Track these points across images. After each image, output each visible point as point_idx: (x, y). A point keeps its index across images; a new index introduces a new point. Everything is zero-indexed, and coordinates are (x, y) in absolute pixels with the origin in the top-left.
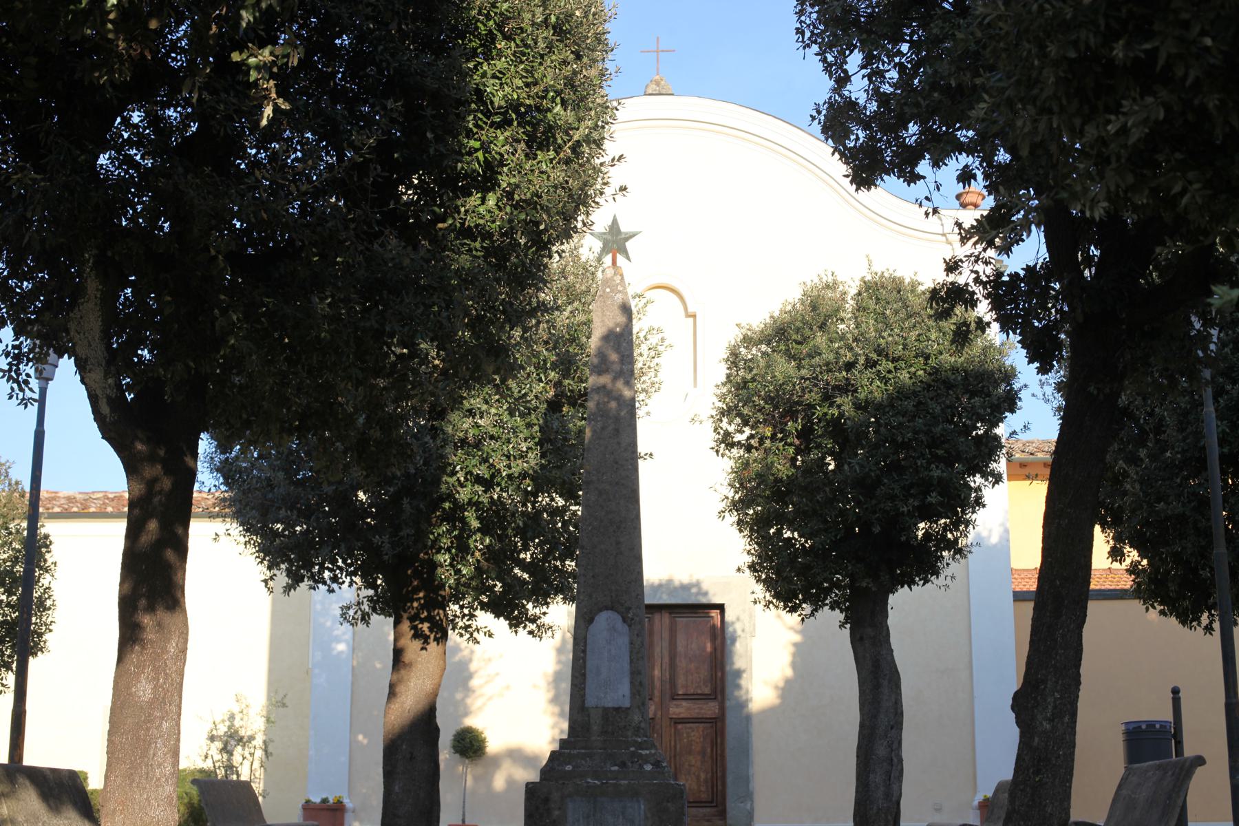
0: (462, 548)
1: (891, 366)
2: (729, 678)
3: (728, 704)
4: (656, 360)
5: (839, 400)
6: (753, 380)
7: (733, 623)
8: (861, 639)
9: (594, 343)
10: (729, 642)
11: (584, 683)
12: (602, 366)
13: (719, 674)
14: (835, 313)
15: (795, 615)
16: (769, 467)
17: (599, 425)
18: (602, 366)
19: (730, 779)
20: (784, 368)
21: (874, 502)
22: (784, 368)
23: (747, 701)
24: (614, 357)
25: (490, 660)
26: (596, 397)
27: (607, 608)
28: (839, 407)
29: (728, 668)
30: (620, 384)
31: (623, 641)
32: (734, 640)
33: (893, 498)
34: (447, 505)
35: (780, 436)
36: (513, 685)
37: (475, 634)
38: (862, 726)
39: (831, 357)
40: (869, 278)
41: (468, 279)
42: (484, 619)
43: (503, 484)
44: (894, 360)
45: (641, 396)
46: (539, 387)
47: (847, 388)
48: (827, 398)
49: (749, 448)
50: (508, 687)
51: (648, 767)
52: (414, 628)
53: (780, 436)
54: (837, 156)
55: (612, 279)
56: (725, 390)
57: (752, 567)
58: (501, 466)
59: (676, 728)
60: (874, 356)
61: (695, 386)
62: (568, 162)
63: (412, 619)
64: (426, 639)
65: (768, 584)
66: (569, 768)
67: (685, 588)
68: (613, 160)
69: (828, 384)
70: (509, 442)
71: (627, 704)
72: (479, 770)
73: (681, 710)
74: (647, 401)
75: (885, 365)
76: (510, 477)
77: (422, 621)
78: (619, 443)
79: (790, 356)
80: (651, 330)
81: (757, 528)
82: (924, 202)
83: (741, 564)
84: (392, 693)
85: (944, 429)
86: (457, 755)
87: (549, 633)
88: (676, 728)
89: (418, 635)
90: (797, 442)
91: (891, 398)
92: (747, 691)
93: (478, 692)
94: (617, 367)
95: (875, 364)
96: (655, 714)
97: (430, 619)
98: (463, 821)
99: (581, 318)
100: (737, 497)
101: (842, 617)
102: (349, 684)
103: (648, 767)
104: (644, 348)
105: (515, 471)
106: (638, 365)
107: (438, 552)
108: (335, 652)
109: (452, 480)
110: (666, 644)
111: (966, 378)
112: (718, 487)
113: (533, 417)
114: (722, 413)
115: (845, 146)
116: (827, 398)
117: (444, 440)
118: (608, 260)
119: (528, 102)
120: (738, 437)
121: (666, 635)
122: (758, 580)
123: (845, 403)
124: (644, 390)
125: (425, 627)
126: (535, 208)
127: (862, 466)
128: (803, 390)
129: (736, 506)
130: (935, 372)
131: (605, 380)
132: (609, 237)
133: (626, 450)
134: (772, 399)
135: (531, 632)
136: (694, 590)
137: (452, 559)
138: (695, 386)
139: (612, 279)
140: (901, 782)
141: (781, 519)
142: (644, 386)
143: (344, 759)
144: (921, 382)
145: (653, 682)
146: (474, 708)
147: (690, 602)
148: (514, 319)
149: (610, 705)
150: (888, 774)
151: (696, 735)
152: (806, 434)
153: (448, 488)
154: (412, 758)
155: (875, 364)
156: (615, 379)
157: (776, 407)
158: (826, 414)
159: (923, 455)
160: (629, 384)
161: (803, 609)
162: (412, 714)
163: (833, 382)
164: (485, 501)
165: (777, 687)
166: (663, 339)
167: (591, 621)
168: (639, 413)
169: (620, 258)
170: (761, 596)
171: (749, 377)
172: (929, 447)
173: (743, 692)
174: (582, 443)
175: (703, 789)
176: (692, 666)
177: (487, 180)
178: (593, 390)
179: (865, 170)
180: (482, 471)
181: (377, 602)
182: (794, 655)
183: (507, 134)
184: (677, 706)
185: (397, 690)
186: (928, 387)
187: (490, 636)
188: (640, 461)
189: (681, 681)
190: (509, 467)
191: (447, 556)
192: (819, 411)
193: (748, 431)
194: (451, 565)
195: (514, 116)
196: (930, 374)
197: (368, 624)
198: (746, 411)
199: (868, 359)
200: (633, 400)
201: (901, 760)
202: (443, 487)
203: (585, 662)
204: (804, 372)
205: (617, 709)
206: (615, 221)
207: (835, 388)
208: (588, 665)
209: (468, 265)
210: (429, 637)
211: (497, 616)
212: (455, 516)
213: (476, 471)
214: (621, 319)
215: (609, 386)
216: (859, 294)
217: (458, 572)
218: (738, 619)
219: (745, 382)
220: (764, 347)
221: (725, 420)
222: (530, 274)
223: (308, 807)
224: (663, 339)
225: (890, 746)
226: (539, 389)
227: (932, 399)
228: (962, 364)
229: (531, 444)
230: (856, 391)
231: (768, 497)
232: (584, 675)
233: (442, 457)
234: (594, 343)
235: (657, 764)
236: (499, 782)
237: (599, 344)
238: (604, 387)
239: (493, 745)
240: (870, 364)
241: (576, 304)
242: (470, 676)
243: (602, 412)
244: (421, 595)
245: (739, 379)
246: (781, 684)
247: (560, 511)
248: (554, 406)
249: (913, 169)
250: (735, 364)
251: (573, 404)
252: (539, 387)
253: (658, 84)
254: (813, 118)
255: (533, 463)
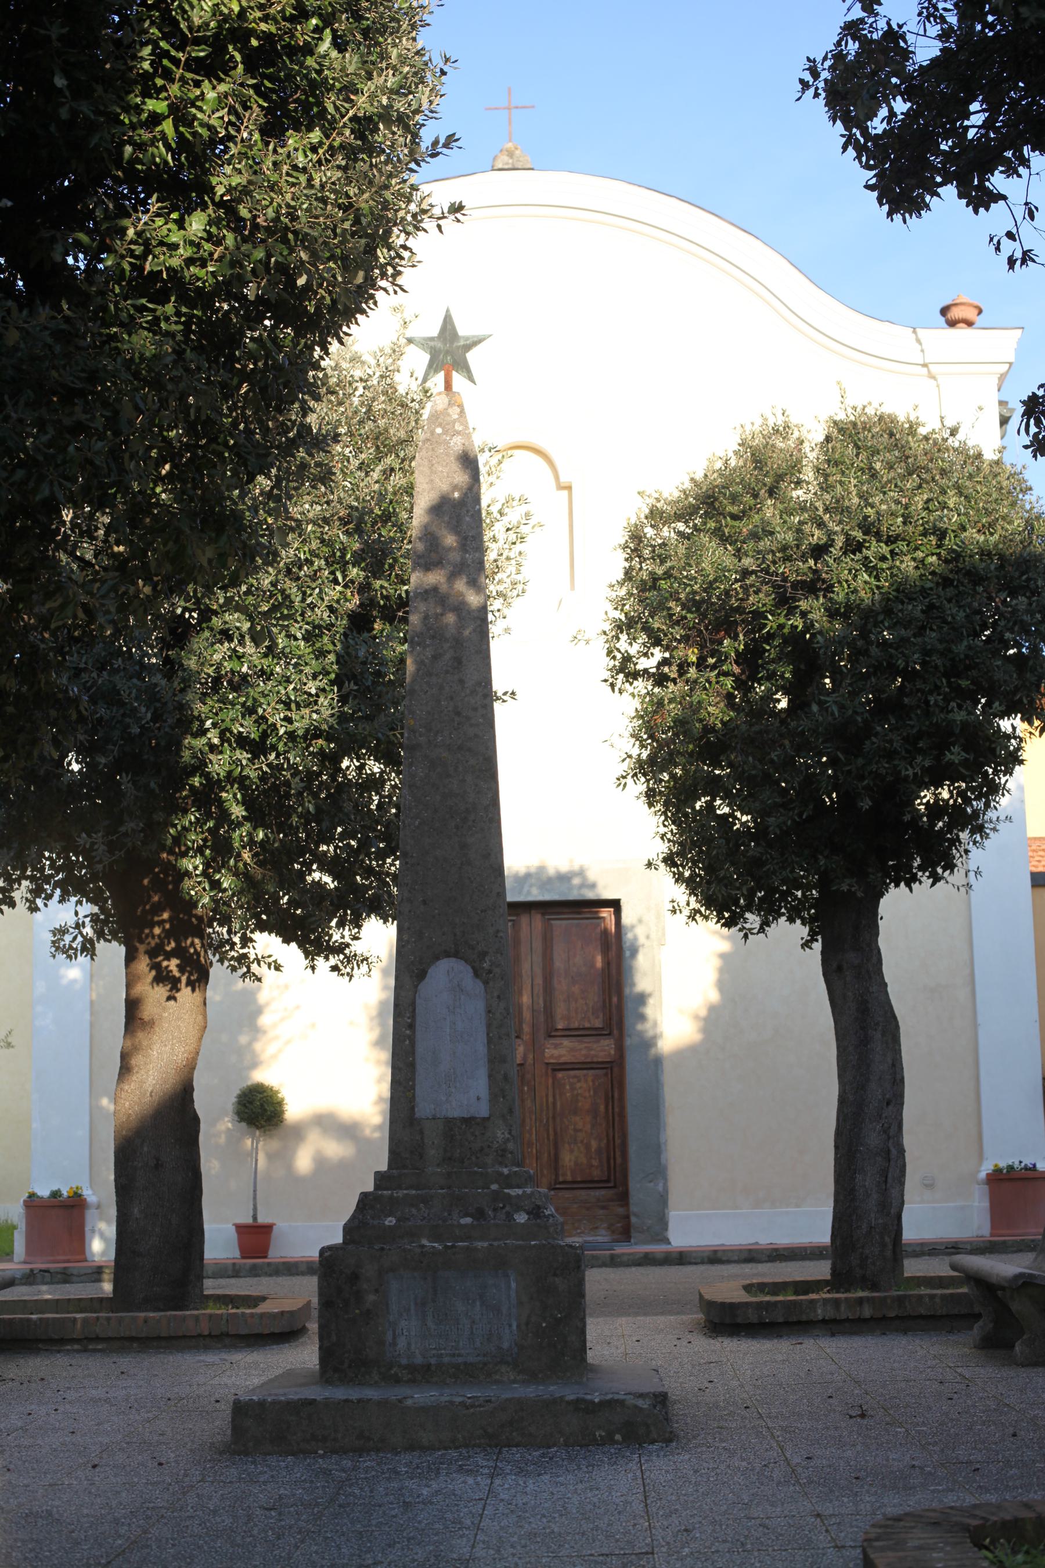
0: (220, 851)
1: (885, 549)
2: (629, 1006)
3: (628, 1042)
4: (519, 547)
5: (803, 605)
6: (667, 575)
7: (633, 927)
8: (840, 969)
9: (419, 517)
10: (628, 954)
11: (413, 1080)
12: (430, 556)
13: (615, 999)
14: (790, 471)
15: (734, 930)
16: (696, 708)
17: (429, 652)
18: (430, 556)
19: (633, 1149)
20: (715, 556)
21: (860, 761)
22: (715, 556)
23: (655, 1038)
24: (450, 540)
25: (286, 987)
26: (422, 607)
27: (447, 954)
28: (804, 614)
29: (627, 991)
30: (460, 585)
31: (475, 1007)
32: (634, 951)
33: (890, 755)
34: (196, 781)
35: (711, 661)
36: (318, 1034)
37: (254, 967)
38: (842, 1101)
39: (790, 537)
40: (841, 416)
41: (148, 374)
42: (266, 943)
43: (281, 747)
44: (891, 540)
45: (496, 604)
46: (333, 593)
47: (813, 586)
48: (784, 601)
49: (660, 679)
50: (313, 1025)
51: (521, 1218)
52: (156, 966)
53: (711, 661)
54: (851, 152)
55: (445, 412)
56: (623, 592)
57: (669, 860)
58: (277, 718)
59: (554, 1078)
60: (858, 535)
61: (573, 587)
62: (351, 153)
63: (152, 953)
64: (174, 984)
65: (692, 885)
66: (390, 1221)
67: (564, 878)
68: (435, 143)
69: (785, 579)
70: (288, 681)
71: (483, 1110)
72: (274, 1144)
73: (563, 1051)
74: (505, 611)
75: (875, 549)
76: (291, 736)
77: (168, 956)
78: (461, 681)
79: (724, 539)
80: (509, 501)
81: (675, 800)
82: (1006, 242)
83: (652, 856)
84: (125, 1069)
85: (969, 648)
86: (244, 1124)
87: (364, 967)
88: (554, 1078)
89: (161, 977)
90: (736, 670)
91: (886, 599)
92: (655, 1024)
93: (271, 1034)
94: (455, 557)
95: (859, 547)
96: (525, 1058)
97: (179, 952)
98: (255, 1218)
99: (397, 480)
100: (645, 754)
101: (804, 931)
102: (87, 1026)
103: (521, 1218)
104: (499, 529)
105: (299, 726)
106: (491, 556)
107: (184, 854)
108: (64, 982)
109: (200, 743)
110: (538, 958)
111: (1001, 567)
112: (615, 740)
113: (326, 639)
114: (619, 627)
115: (865, 132)
116: (784, 601)
117: (183, 680)
118: (437, 382)
119: (263, 26)
120: (643, 664)
121: (538, 945)
122: (679, 878)
123: (814, 608)
124: (500, 594)
125: (173, 964)
126: (285, 241)
127: (842, 707)
128: (745, 589)
129: (646, 768)
130: (955, 557)
131: (435, 578)
132: (439, 345)
133: (473, 692)
134: (698, 604)
135: (335, 968)
136: (576, 881)
137: (207, 865)
138: (573, 587)
139: (445, 412)
140: (902, 1184)
141: (714, 787)
142: (500, 588)
143: (83, 1133)
144: (933, 573)
145: (520, 1012)
146: (265, 1056)
147: (571, 897)
148: (252, 459)
149: (456, 1114)
150: (884, 1174)
151: (583, 1087)
152: (751, 660)
153: (194, 756)
154: (158, 1166)
155: (859, 547)
156: (452, 577)
157: (703, 616)
158: (781, 627)
159: (937, 688)
160: (475, 584)
161: (746, 920)
162: (156, 1098)
163: (793, 577)
164: (253, 775)
165: (696, 1017)
166: (528, 515)
167: (422, 975)
168: (494, 630)
169: (457, 378)
170: (683, 903)
171: (660, 571)
172: (946, 675)
173: (648, 1025)
174: (401, 682)
175: (595, 1163)
176: (576, 989)
177: (183, 186)
178: (417, 595)
179: (902, 185)
180: (247, 727)
181: (105, 922)
182: (721, 971)
183: (222, 88)
184: (556, 1046)
185: (133, 1062)
186: (946, 582)
187: (278, 968)
188: (497, 706)
189: (560, 1010)
190: (288, 720)
191: (198, 861)
192: (771, 623)
193: (659, 654)
194: (204, 873)
195: (238, 57)
196: (946, 561)
197: (93, 955)
198: (656, 624)
199: (849, 539)
200: (484, 609)
201: (902, 1151)
202: (186, 754)
203: (413, 1044)
204: (747, 562)
205: (468, 1121)
206: (448, 321)
207: (795, 585)
208: (420, 1049)
209: (151, 350)
210: (179, 980)
211: (287, 941)
212: (208, 797)
213: (237, 728)
214: (461, 478)
215: (444, 588)
216: (828, 439)
217: (216, 885)
218: (640, 921)
219: (655, 579)
220: (681, 526)
221: (624, 637)
222: (290, 380)
223: (33, 1203)
224: (528, 515)
225: (885, 1131)
226: (333, 597)
227: (949, 601)
228: (996, 545)
229: (323, 683)
230: (830, 589)
231: (691, 754)
232: (412, 1066)
233: (182, 707)
234: (419, 517)
235: (536, 1212)
236: (303, 1161)
237: (426, 519)
238: (435, 589)
239: (294, 1110)
240: (853, 547)
241: (390, 460)
242: (259, 1011)
243: (433, 632)
244: (166, 916)
245: (645, 575)
246: (703, 1013)
247: (375, 783)
248: (360, 621)
249: (982, 181)
250: (636, 552)
251: (389, 617)
252: (333, 593)
253: (511, 154)
254: (805, 85)
255: (326, 713)
